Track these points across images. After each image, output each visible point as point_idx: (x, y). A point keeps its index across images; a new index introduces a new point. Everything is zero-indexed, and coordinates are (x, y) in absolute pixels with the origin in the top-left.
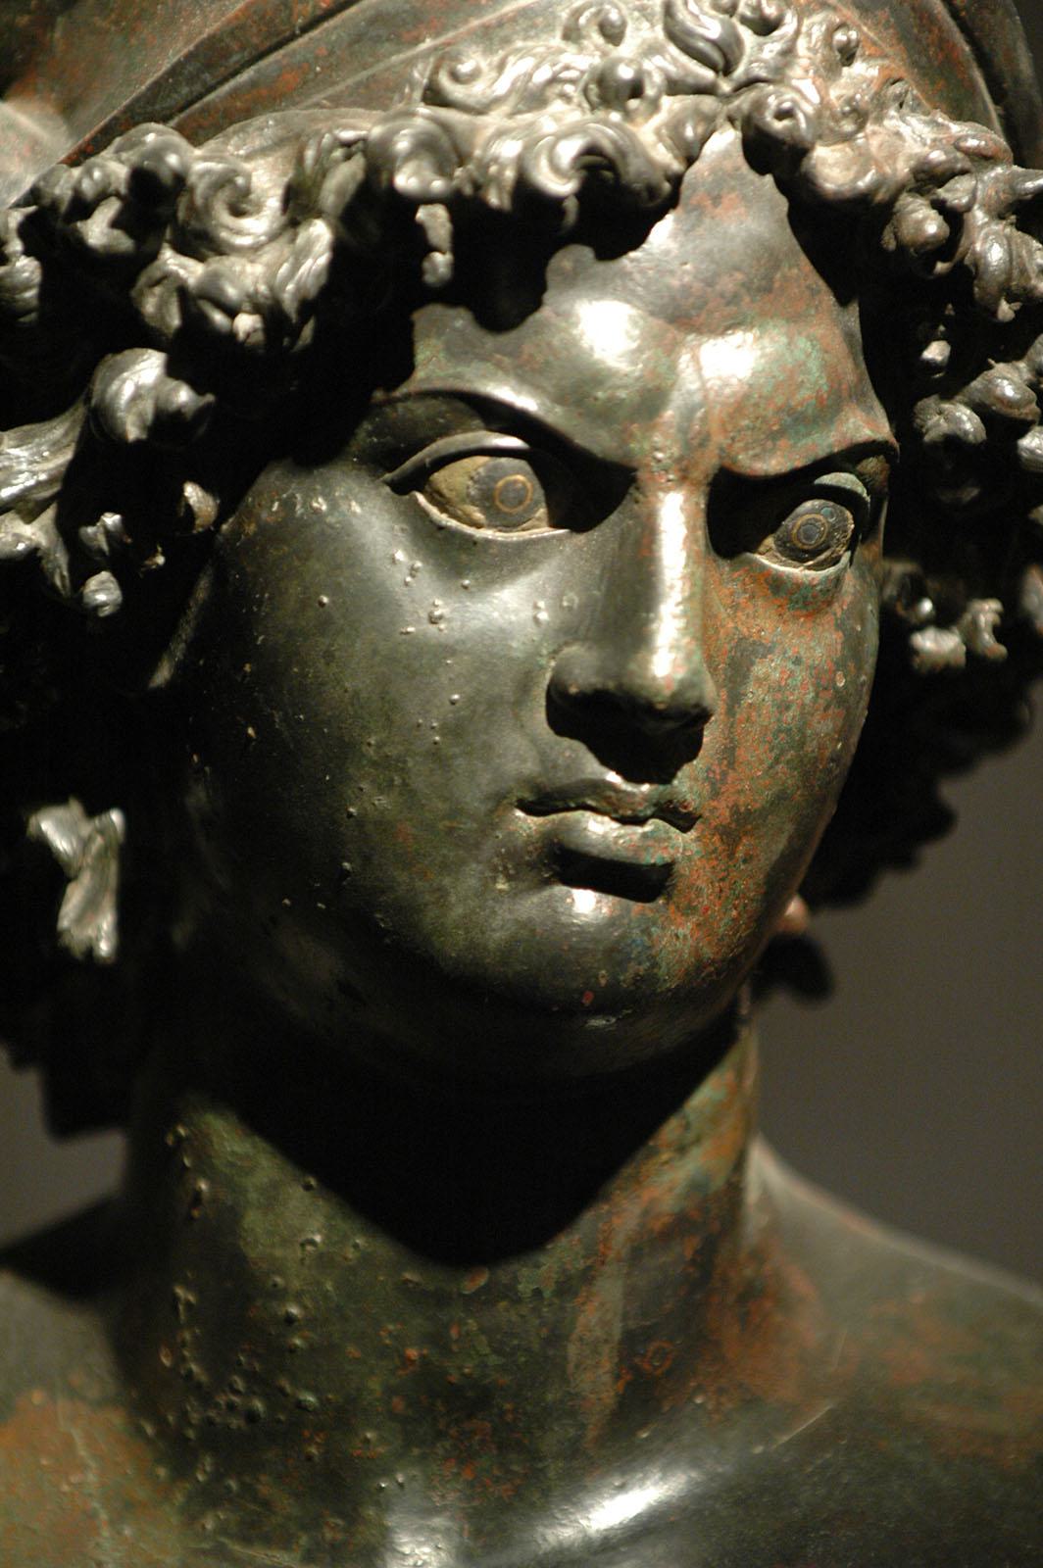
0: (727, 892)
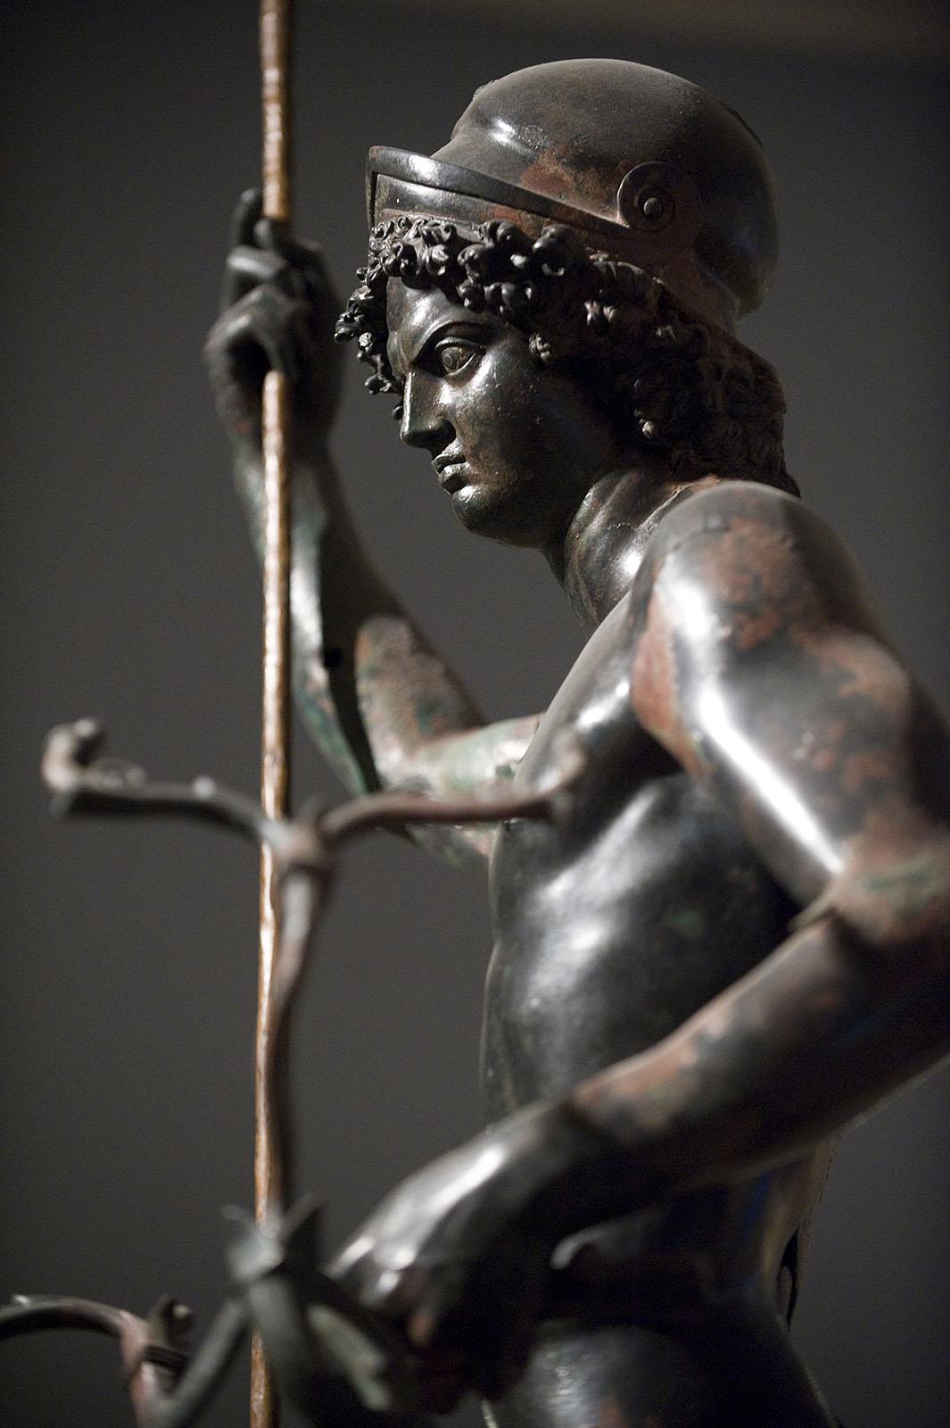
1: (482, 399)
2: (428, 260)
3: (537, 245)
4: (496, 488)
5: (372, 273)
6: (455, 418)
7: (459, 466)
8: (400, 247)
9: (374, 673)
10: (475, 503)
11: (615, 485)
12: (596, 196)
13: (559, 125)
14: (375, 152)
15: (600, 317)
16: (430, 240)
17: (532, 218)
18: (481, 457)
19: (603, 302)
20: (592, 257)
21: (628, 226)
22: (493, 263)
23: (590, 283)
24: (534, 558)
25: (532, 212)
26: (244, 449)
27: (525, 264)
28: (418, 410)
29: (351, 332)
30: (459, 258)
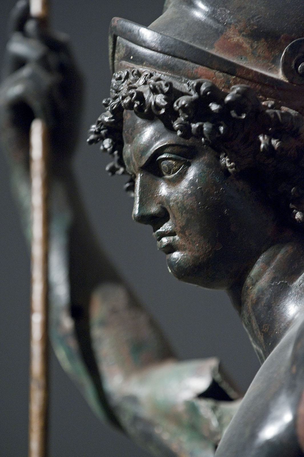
0: (191, 243)
1: (188, 196)
2: (153, 103)
3: (228, 98)
4: (197, 254)
5: (114, 104)
6: (169, 206)
7: (171, 238)
8: (133, 94)
9: (103, 323)
10: (182, 264)
11: (277, 254)
12: (265, 58)
13: (240, 8)
14: (116, 22)
15: (270, 146)
16: (154, 91)
17: (223, 75)
18: (187, 234)
19: (272, 136)
20: (263, 103)
21: (287, 81)
22: (198, 109)
23: (261, 122)
24: (221, 295)
25: (224, 72)
26: (17, 173)
27: (219, 110)
28: (144, 200)
29: (98, 138)
30: (175, 105)
